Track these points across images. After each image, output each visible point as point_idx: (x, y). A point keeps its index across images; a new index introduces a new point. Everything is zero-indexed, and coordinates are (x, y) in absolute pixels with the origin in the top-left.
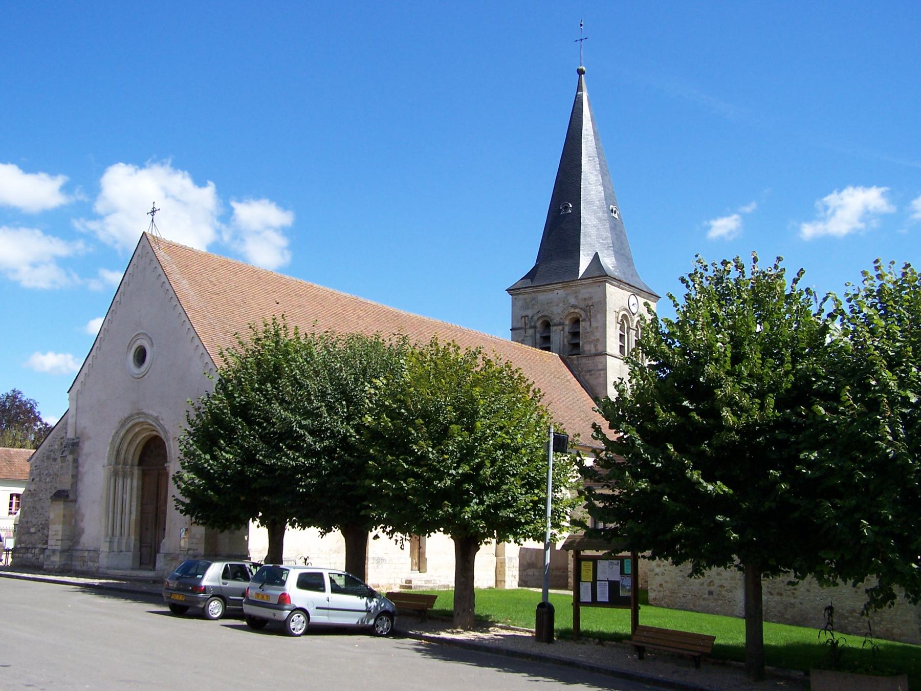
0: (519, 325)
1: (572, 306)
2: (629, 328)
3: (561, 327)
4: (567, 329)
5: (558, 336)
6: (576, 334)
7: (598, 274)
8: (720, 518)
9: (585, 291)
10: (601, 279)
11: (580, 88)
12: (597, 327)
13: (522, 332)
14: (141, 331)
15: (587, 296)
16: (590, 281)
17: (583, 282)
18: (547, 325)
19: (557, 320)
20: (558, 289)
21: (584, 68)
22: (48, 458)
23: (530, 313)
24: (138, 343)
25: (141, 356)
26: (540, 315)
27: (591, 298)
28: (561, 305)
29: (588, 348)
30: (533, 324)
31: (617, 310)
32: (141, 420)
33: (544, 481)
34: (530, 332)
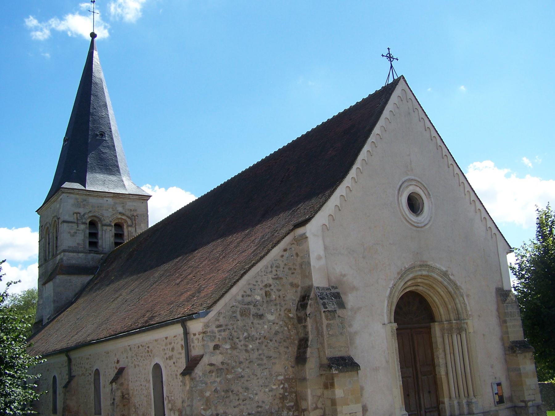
1: (120, 213)
8: (36, 386)
9: (131, 204)
14: (413, 177)
15: (132, 208)
22: (244, 313)
23: (82, 211)
24: (411, 189)
25: (414, 204)
27: (135, 210)
28: (110, 210)
32: (424, 273)
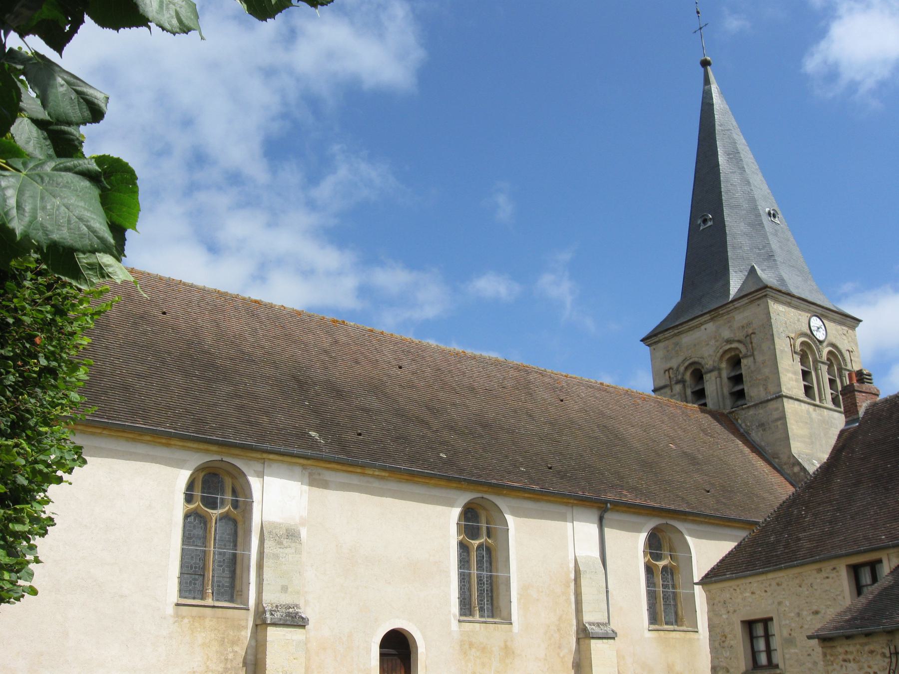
0: (662, 383)
2: (816, 361)
3: (715, 373)
4: (725, 374)
5: (715, 386)
6: (737, 379)
7: (759, 292)
10: (759, 294)
11: (707, 81)
12: (764, 362)
13: (667, 390)
16: (745, 300)
17: (737, 304)
18: (699, 375)
19: (709, 363)
20: (706, 322)
21: (709, 58)
23: (674, 363)
26: (686, 364)
28: (712, 342)
29: (754, 392)
30: (679, 377)
31: (793, 335)
33: (493, 617)
34: (678, 388)
